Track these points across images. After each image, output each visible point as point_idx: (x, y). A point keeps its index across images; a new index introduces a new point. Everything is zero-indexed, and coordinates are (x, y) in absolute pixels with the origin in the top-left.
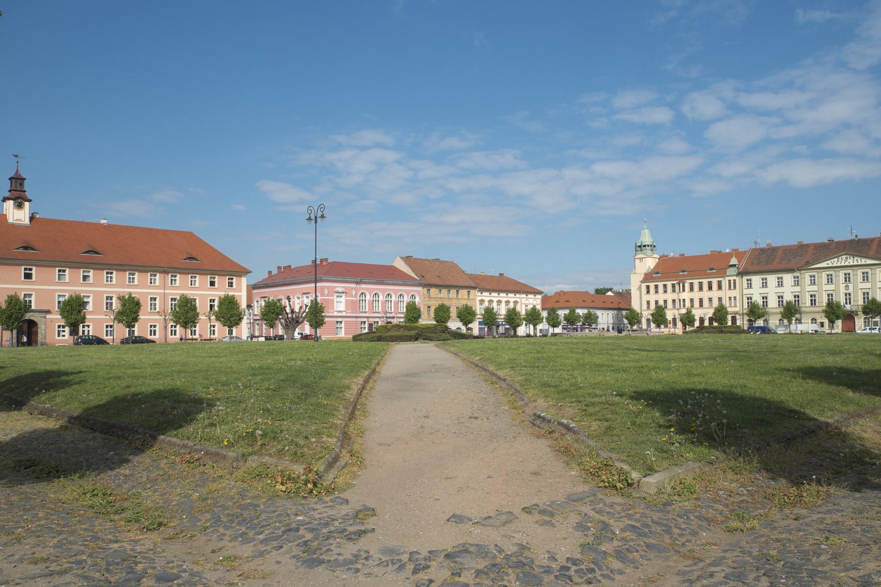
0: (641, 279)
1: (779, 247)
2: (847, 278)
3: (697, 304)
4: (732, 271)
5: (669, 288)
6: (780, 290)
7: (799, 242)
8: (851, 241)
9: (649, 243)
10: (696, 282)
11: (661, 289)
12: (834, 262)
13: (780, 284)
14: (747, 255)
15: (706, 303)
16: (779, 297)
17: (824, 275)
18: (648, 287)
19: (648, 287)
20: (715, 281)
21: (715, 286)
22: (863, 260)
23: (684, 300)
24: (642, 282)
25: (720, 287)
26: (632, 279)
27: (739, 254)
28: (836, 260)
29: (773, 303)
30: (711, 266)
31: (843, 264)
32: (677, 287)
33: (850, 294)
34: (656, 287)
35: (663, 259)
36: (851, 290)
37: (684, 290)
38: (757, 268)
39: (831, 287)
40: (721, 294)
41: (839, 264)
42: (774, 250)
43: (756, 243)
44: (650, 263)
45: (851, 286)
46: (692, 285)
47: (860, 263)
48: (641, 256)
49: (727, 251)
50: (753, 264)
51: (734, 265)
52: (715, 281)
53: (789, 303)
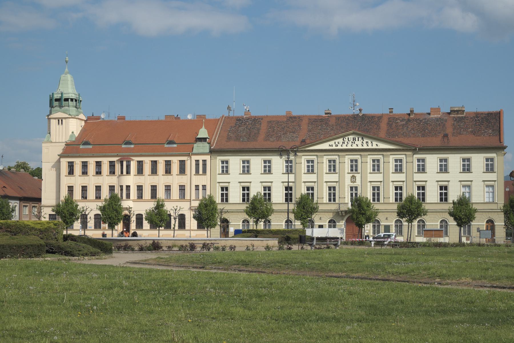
0: (60, 152)
1: (262, 118)
2: (354, 167)
3: (175, 193)
4: (199, 147)
5: (105, 168)
6: (246, 178)
7: (288, 112)
8: (355, 117)
9: (74, 96)
10: (147, 161)
11: (92, 168)
12: (339, 143)
13: (246, 170)
14: (220, 125)
15: (91, 193)
16: (441, 188)
17: (325, 159)
18: (71, 166)
19: (71, 166)
20: (175, 161)
21: (175, 168)
22: (375, 143)
23: (128, 187)
24: (61, 156)
25: (182, 170)
26: (44, 151)
27: (211, 125)
28: (341, 140)
29: (278, 196)
30: (170, 138)
31: (349, 147)
32: (118, 167)
33: (356, 188)
34: (99, 164)
35: (92, 122)
36: (358, 183)
37: (128, 172)
38: (237, 145)
39: (334, 177)
40: (184, 180)
41: (344, 147)
42: (256, 120)
43: (229, 108)
44: (74, 127)
45: (358, 176)
46: (140, 164)
47: (370, 147)
48: (60, 115)
49: (189, 117)
50: (229, 138)
51: (204, 139)
52: (175, 161)
53: (410, 199)
